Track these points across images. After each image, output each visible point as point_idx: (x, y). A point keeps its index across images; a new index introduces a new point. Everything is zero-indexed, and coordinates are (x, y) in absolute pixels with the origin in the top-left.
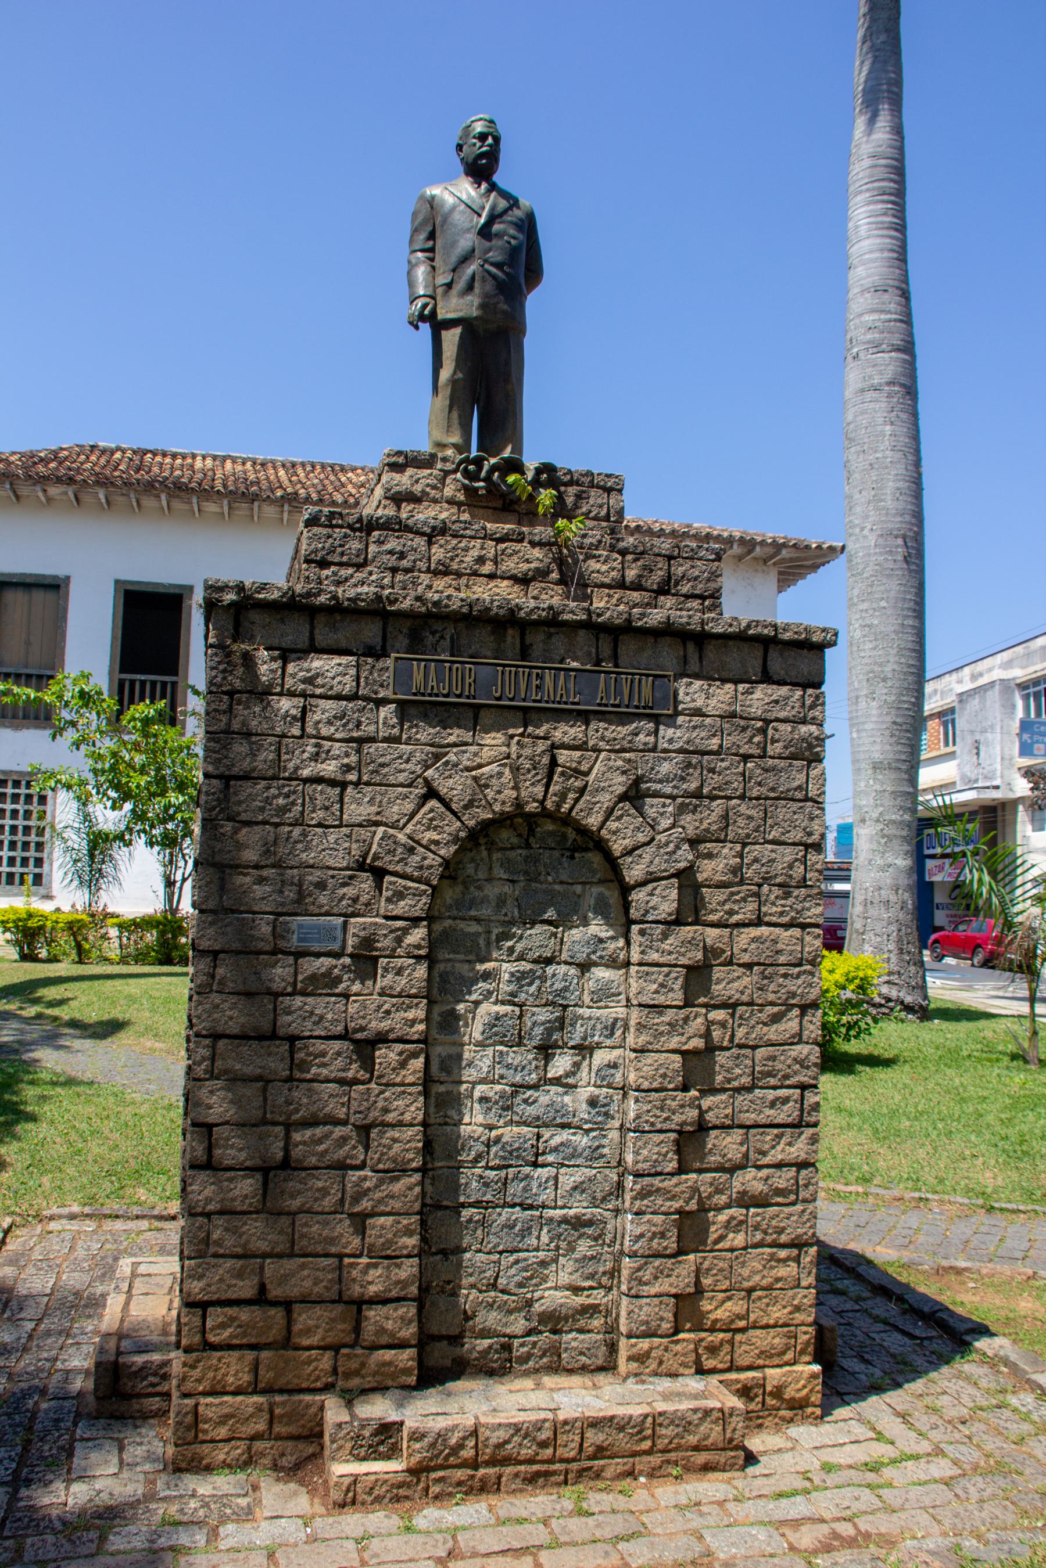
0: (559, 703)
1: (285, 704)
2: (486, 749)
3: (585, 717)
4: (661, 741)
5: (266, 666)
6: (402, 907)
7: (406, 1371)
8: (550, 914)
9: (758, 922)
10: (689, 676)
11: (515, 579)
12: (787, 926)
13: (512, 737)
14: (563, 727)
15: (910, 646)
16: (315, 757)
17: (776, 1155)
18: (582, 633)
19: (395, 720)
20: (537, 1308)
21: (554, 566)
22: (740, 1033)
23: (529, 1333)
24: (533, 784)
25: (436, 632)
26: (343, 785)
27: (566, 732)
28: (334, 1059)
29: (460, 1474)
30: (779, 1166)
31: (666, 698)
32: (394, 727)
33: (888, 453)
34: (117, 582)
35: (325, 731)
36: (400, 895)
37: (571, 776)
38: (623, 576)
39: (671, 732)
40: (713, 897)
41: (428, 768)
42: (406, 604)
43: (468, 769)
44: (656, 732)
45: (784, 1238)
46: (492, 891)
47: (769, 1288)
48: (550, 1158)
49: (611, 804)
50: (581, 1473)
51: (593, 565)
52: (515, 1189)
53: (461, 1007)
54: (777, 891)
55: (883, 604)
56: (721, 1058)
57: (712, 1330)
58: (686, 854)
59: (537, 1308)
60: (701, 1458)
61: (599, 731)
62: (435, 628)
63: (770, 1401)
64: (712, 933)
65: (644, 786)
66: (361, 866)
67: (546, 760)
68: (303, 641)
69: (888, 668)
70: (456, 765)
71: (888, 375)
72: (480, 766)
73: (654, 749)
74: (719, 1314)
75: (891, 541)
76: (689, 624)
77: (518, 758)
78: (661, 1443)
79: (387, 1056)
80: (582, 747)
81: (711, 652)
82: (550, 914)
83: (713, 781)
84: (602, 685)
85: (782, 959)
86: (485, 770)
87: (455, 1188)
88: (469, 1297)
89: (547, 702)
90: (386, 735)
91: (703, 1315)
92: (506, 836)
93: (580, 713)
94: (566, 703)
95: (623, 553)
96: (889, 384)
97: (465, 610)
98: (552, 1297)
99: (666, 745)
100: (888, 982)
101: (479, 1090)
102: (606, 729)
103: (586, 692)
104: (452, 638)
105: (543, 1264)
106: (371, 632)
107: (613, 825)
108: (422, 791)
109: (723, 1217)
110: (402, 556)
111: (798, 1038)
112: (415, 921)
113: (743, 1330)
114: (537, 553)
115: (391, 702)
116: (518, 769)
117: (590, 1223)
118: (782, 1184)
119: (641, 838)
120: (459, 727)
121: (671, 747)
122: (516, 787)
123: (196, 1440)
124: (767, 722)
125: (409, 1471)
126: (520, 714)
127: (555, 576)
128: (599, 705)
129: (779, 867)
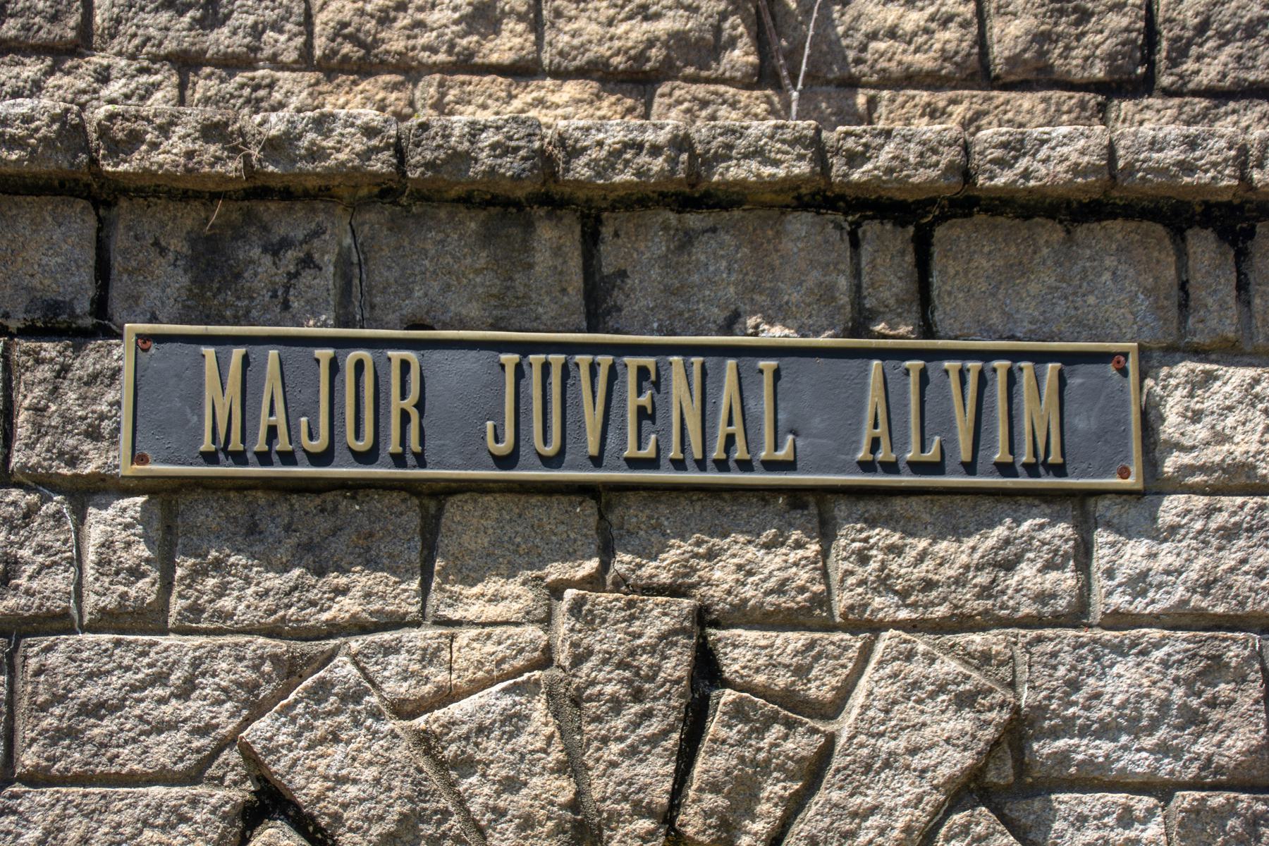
0: (722, 465)
2: (464, 636)
3: (816, 509)
4: (1100, 584)
10: (1199, 353)
13: (556, 590)
14: (739, 549)
18: (800, 223)
19: (142, 550)
21: (735, 25)
24: (632, 752)
25: (286, 244)
27: (752, 565)
31: (1111, 433)
32: (136, 573)
37: (772, 719)
38: (982, 42)
39: (1135, 553)
41: (258, 710)
42: (170, 154)
43: (403, 710)
44: (1083, 554)
49: (921, 816)
61: (869, 562)
62: (280, 230)
65: (1044, 749)
67: (676, 665)
70: (356, 696)
72: (447, 696)
73: (1077, 616)
76: (1187, 167)
77: (578, 660)
80: (810, 615)
84: (874, 397)
86: (456, 710)
89: (679, 465)
90: (110, 602)
93: (797, 497)
94: (745, 466)
97: (380, 164)
99: (1119, 600)
102: (896, 550)
103: (817, 423)
104: (344, 265)
108: (237, 795)
115: (126, 488)
116: (577, 702)
120: (372, 564)
121: (1139, 605)
122: (571, 766)
126: (587, 511)
127: (741, 56)
128: (866, 467)
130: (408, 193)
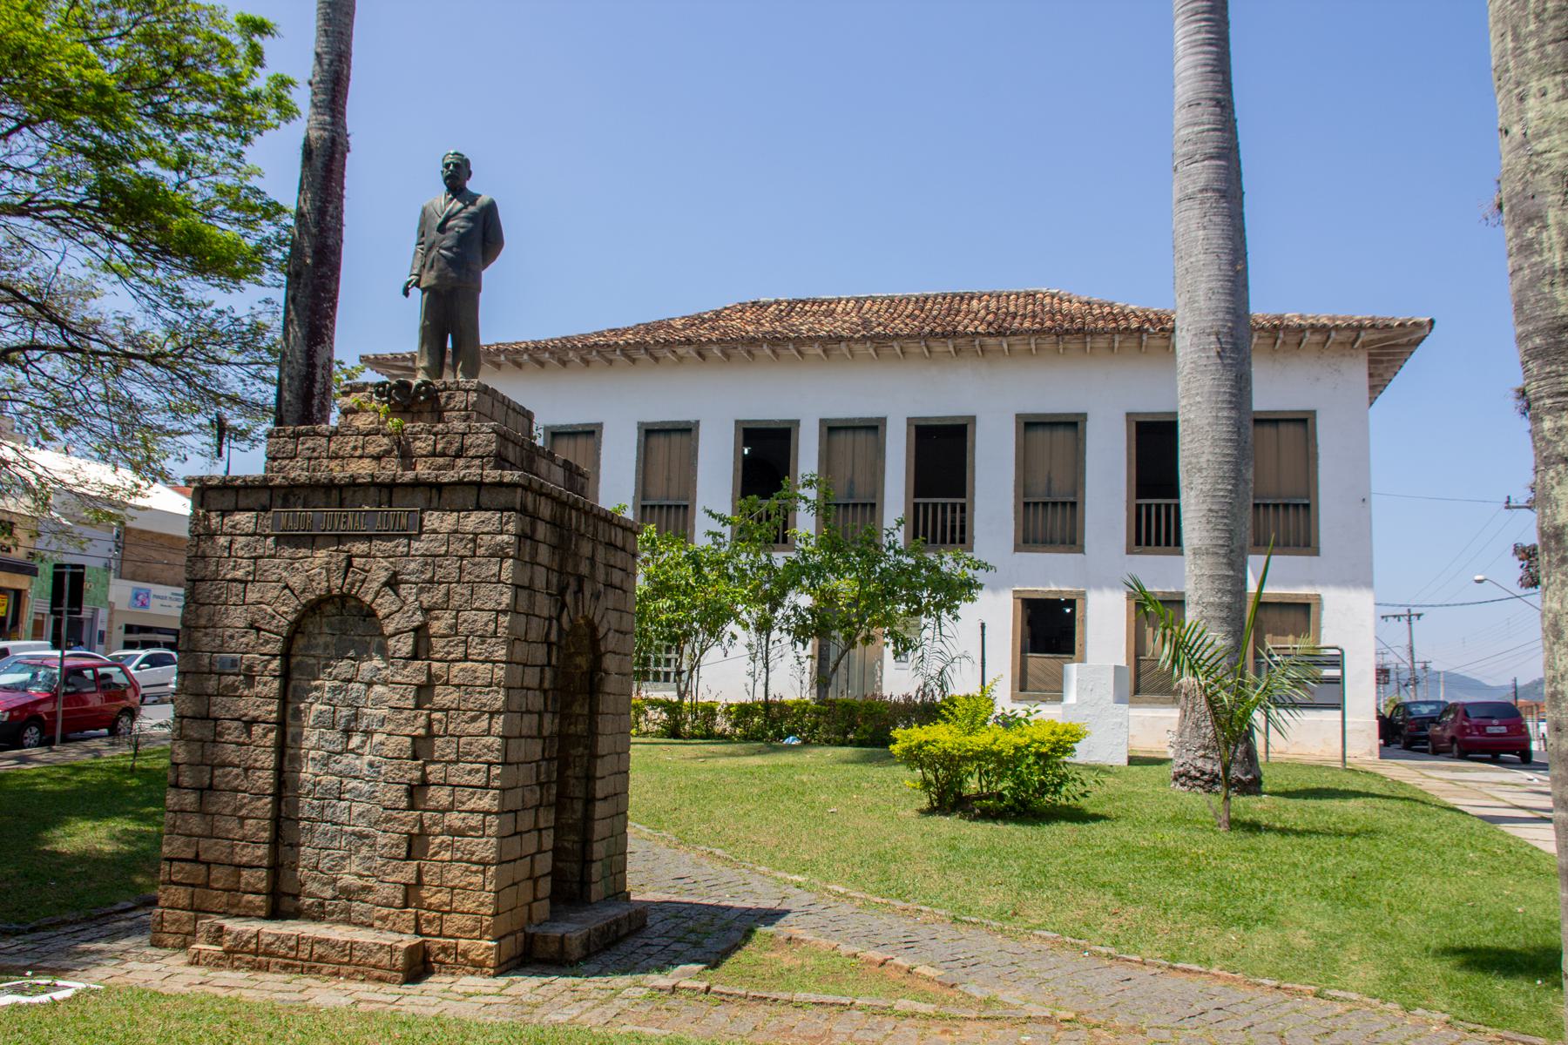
1: (223, 541)
3: (369, 538)
5: (215, 520)
6: (268, 649)
7: (260, 908)
8: (352, 653)
9: (466, 659)
11: (372, 457)
12: (483, 662)
14: (358, 545)
15: (1225, 436)
16: (234, 568)
17: (470, 805)
20: (339, 884)
22: (451, 727)
23: (334, 898)
26: (246, 582)
27: (360, 547)
28: (233, 732)
29: (249, 957)
30: (472, 811)
33: (1202, 257)
34: (737, 422)
35: (240, 553)
36: (267, 642)
40: (438, 643)
42: (278, 481)
45: (474, 858)
46: (321, 640)
47: (464, 888)
48: (347, 796)
50: (311, 969)
51: (418, 444)
52: (328, 812)
53: (302, 706)
54: (477, 640)
55: (1198, 399)
56: (438, 742)
57: (428, 909)
58: (418, 618)
59: (339, 884)
60: (377, 973)
63: (460, 959)
64: (435, 665)
66: (251, 626)
68: (232, 506)
69: (1203, 459)
71: (1201, 184)
74: (433, 900)
75: (1205, 339)
78: (355, 959)
79: (258, 730)
80: (367, 556)
81: (446, 495)
82: (352, 653)
83: (440, 573)
85: (478, 682)
87: (297, 808)
88: (302, 873)
91: (423, 899)
92: (329, 609)
95: (436, 434)
96: (1201, 191)
98: (348, 879)
100: (1203, 756)
101: (312, 754)
105: (343, 858)
106: (264, 498)
107: (379, 601)
109: (438, 841)
110: (314, 450)
111: (488, 732)
112: (274, 656)
113: (449, 912)
114: (386, 440)
117: (367, 836)
118: (473, 823)
119: (394, 608)
123: (161, 931)
124: (476, 535)
125: (225, 951)
129: (479, 625)
130: (314, 486)
